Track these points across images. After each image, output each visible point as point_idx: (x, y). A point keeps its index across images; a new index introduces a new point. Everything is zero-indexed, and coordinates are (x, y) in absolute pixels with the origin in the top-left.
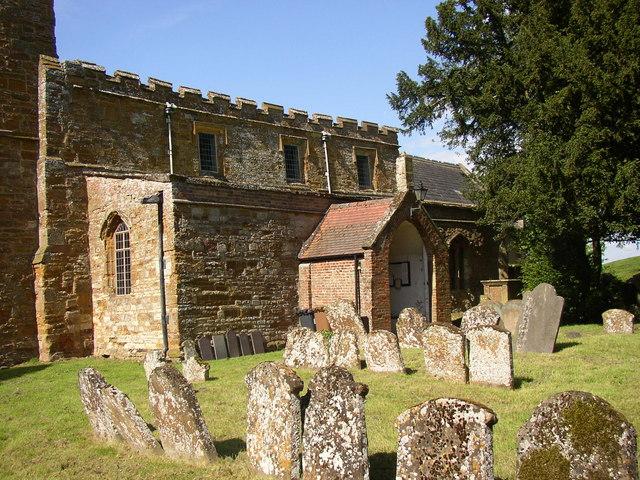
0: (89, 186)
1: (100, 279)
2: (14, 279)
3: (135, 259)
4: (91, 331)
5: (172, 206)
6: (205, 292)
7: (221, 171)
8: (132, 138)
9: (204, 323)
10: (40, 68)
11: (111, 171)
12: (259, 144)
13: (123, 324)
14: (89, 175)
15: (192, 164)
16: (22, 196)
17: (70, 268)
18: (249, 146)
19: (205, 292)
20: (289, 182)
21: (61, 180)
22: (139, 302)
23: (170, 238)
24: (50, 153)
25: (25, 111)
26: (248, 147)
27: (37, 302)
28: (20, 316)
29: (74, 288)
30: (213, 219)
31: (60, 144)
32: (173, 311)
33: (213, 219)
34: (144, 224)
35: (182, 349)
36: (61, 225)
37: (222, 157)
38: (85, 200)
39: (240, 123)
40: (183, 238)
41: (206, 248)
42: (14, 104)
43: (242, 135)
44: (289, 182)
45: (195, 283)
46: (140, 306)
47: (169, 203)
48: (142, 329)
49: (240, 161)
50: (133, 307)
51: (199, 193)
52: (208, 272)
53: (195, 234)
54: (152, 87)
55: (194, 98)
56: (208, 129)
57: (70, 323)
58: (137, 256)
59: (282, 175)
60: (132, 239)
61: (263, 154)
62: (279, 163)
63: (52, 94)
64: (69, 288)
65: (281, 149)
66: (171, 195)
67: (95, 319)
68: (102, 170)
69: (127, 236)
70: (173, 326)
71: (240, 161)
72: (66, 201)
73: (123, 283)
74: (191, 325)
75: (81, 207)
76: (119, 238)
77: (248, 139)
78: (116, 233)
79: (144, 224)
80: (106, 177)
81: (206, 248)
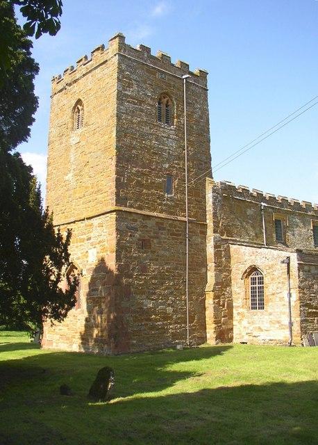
0: (231, 249)
1: (240, 300)
2: (197, 299)
3: (267, 292)
4: (232, 329)
5: (297, 265)
6: (310, 310)
7: (285, 240)
8: (247, 223)
9: (310, 326)
10: (207, 185)
11: (252, 243)
12: (301, 225)
13: (258, 325)
14: (232, 244)
15: (272, 237)
16: (201, 255)
17: (224, 294)
18: (297, 226)
19: (310, 310)
20: (316, 247)
21: (219, 247)
22: (270, 314)
23: (295, 282)
24: (215, 232)
25: (200, 208)
26: (296, 228)
27: (207, 313)
28: (199, 320)
29: (226, 305)
30: (313, 272)
31: (218, 227)
32: (297, 320)
33: (313, 272)
34: (275, 273)
35: (302, 339)
36: (220, 271)
37: (285, 234)
38: (230, 257)
39: (293, 213)
40: (301, 282)
41: (310, 287)
42: (196, 204)
43: (294, 220)
44: (316, 247)
45: (306, 305)
46: (271, 317)
47: (295, 263)
48: (272, 328)
49: (294, 235)
50: (267, 317)
51: (307, 258)
52: (311, 300)
53: (306, 280)
54: (255, 194)
55: (272, 199)
56: (279, 217)
57: (224, 324)
58: (270, 290)
59: (313, 243)
60: (266, 280)
61: (304, 230)
62: (311, 236)
63: (215, 199)
64: (224, 306)
65: (312, 228)
66: (296, 260)
67: (234, 323)
68: (236, 241)
69: (261, 278)
70: (296, 328)
71: (294, 235)
72: (221, 258)
73: (258, 301)
74: (305, 327)
75: (228, 261)
76: (254, 279)
77: (296, 222)
78: (251, 276)
79: (275, 273)
80: (246, 246)
81: (310, 287)
